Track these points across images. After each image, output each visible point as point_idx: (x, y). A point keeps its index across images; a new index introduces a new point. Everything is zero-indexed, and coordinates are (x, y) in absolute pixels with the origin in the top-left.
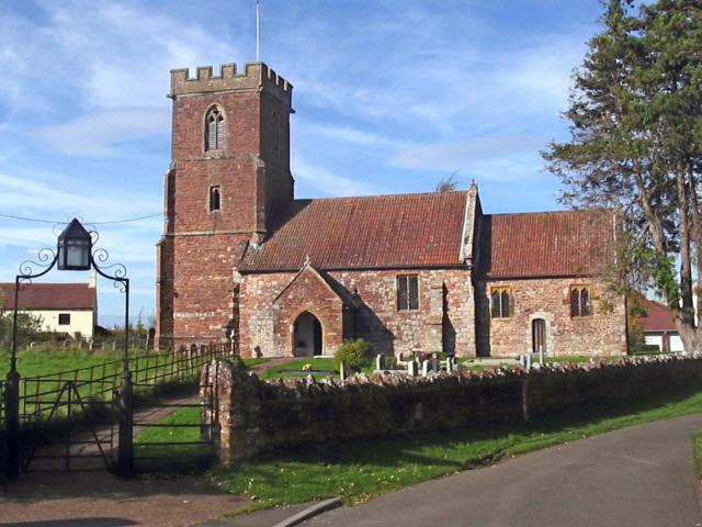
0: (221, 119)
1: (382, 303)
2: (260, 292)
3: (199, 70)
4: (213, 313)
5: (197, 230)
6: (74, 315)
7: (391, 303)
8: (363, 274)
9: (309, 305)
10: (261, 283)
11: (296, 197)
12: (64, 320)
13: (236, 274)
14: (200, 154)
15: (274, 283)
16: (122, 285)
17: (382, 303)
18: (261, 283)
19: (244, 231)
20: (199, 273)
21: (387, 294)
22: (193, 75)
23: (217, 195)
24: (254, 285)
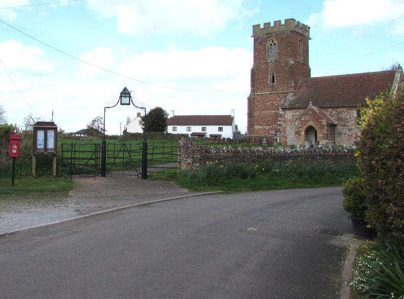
0: (275, 44)
1: (348, 122)
2: (291, 117)
3: (265, 24)
4: (271, 126)
5: (264, 92)
6: (225, 128)
7: (352, 122)
8: (339, 110)
9: (311, 123)
10: (292, 114)
11: (314, 74)
12: (220, 129)
13: (280, 110)
14: (265, 60)
15: (298, 113)
16: (107, 109)
17: (348, 122)
18: (292, 114)
19: (284, 92)
20: (265, 110)
21: (350, 118)
22: (262, 27)
23: (273, 77)
24: (289, 115)
